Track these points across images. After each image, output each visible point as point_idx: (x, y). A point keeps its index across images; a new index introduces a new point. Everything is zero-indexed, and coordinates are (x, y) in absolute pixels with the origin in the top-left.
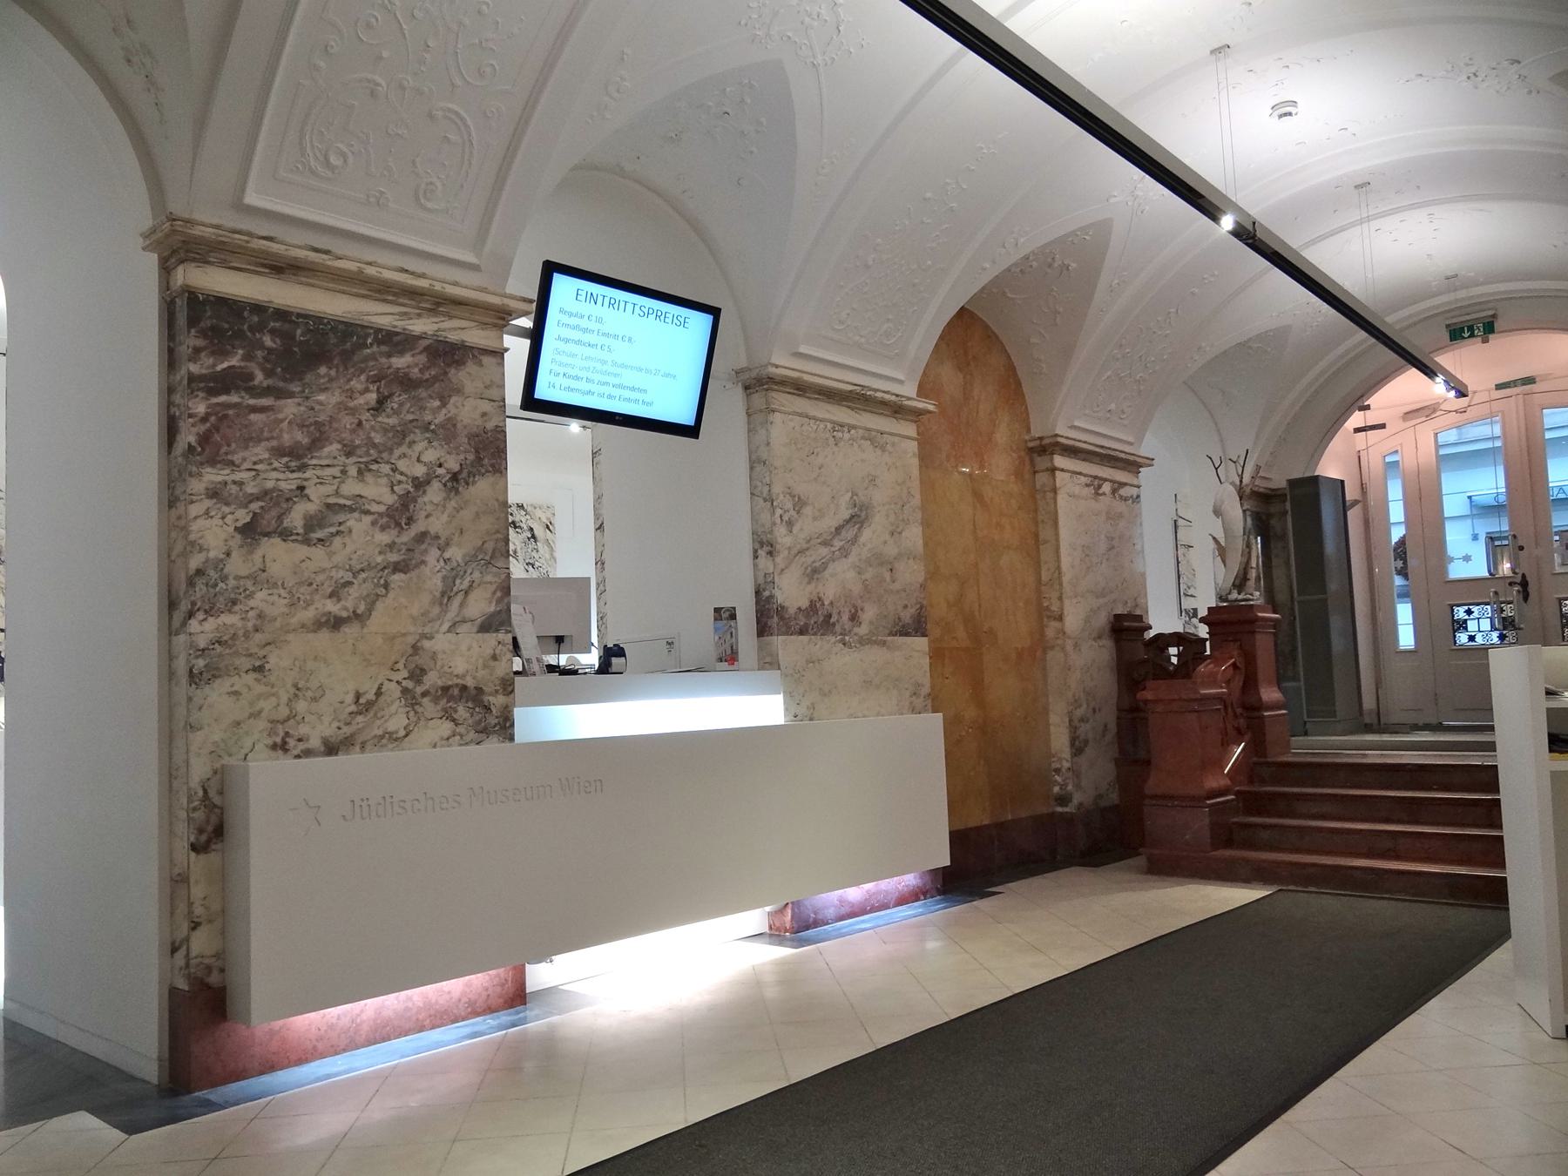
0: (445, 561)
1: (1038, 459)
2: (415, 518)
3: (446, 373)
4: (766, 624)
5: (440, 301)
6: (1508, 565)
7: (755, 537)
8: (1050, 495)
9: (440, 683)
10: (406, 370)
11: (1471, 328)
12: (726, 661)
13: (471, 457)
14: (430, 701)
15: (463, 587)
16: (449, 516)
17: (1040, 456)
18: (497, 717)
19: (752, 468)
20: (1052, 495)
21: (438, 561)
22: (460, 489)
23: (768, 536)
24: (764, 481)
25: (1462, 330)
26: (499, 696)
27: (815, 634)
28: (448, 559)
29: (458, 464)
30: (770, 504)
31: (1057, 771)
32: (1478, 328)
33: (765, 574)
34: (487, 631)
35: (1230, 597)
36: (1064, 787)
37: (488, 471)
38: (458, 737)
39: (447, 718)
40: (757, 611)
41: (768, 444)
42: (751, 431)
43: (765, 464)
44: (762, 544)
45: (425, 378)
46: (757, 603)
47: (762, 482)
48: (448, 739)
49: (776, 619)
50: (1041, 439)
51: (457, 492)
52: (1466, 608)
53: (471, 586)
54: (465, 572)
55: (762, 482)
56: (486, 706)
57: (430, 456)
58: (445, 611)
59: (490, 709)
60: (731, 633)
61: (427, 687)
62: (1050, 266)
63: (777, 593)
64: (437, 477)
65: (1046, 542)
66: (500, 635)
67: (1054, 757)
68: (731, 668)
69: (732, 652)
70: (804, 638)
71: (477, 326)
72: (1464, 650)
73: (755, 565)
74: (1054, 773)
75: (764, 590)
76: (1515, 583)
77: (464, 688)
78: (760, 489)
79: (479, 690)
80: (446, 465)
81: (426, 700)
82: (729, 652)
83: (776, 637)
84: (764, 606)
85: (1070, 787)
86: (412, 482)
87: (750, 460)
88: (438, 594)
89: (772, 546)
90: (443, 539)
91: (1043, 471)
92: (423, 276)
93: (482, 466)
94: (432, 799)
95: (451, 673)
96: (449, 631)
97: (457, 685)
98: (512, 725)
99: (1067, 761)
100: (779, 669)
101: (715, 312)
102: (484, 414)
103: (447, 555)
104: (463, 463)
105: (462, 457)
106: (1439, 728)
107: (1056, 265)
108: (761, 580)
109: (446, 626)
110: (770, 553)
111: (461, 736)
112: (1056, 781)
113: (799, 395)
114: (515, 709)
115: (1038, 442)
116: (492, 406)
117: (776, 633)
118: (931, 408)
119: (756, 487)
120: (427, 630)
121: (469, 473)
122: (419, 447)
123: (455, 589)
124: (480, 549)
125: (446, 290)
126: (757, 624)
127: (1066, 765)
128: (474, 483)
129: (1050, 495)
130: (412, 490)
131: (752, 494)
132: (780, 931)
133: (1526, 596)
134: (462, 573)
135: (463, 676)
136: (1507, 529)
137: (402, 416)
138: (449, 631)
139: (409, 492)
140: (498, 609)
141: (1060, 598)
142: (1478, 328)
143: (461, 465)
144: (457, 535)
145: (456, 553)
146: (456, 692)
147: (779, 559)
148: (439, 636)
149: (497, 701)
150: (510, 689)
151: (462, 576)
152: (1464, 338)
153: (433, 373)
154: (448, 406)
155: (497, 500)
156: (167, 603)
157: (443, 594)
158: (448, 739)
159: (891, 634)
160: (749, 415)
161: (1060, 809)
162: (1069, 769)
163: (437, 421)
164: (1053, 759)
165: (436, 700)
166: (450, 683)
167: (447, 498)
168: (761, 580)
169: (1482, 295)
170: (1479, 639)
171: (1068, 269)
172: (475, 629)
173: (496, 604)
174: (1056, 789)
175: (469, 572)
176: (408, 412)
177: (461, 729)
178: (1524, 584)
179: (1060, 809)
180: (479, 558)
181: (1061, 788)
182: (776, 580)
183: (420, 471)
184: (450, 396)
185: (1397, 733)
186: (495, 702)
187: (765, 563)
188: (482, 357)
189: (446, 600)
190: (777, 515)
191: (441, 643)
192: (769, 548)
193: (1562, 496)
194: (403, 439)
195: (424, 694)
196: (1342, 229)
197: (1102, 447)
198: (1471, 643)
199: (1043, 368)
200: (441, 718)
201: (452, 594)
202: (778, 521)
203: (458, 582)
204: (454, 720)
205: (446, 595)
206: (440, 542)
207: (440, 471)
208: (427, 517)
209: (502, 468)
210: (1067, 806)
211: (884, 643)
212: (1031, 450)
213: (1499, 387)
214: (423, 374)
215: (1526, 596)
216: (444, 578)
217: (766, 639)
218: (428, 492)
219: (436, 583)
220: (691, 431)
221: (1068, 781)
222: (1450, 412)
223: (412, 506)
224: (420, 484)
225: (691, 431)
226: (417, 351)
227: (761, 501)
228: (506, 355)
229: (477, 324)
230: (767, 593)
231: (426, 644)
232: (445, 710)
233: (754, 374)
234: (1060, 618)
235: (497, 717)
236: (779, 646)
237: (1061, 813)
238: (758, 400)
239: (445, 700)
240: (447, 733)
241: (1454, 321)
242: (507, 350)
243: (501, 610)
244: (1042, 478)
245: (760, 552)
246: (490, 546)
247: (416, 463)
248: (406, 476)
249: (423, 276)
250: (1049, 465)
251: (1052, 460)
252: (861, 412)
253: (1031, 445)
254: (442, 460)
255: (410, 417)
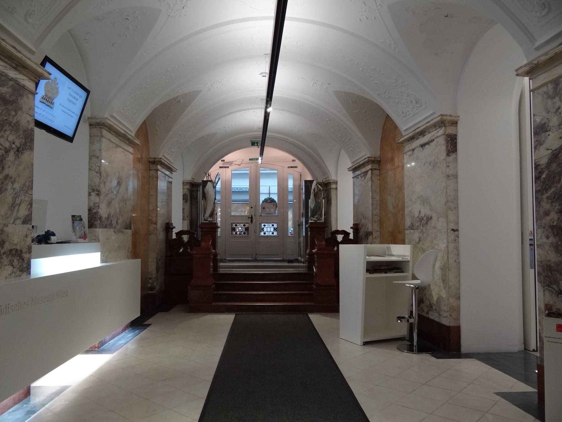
0: (13, 189)
1: (151, 166)
2: (5, 167)
3: (17, 99)
4: (93, 223)
5: (19, 64)
6: (220, 209)
7: (90, 187)
8: (155, 179)
9: (9, 248)
10: (5, 95)
11: (257, 143)
12: (82, 238)
13: (23, 141)
14: (6, 257)
15: (18, 202)
16: (15, 168)
17: (152, 164)
18: (26, 264)
19: (90, 159)
20: (156, 179)
21: (11, 189)
22: (20, 155)
23: (97, 187)
24: (97, 165)
25: (255, 143)
26: (27, 254)
27: (108, 228)
28: (14, 189)
29: (19, 144)
30: (99, 175)
31: (150, 278)
32: (259, 144)
33: (95, 203)
34: (25, 224)
35: (208, 220)
36: (152, 284)
37: (28, 149)
38: (14, 274)
39: (11, 265)
40: (88, 217)
41: (100, 150)
42: (91, 143)
43: (98, 158)
44: (93, 190)
45: (11, 99)
46: (89, 214)
47: (96, 165)
48: (11, 275)
49: (99, 221)
50: (155, 158)
51: (19, 157)
52: (264, 224)
53: (21, 202)
54: (19, 195)
55: (96, 165)
56: (23, 259)
57: (11, 138)
58: (12, 214)
59: (24, 260)
60: (84, 227)
61: (5, 250)
62: (175, 100)
63: (100, 211)
64: (13, 148)
65: (152, 196)
66: (28, 225)
67: (149, 273)
68: (85, 241)
69: (85, 235)
70: (106, 229)
71: (28, 80)
72: (262, 236)
73: (89, 199)
74: (149, 279)
75: (93, 209)
76: (250, 218)
77: (17, 250)
78: (94, 168)
79: (21, 251)
80: (15, 143)
81: (4, 256)
82: (83, 234)
83: (98, 229)
84: (93, 216)
85: (155, 284)
86: (5, 149)
87: (89, 155)
88: (10, 205)
89: (99, 192)
90: (13, 179)
91: (154, 170)
92: (19, 52)
93: (26, 146)
94: (21, 304)
95: (13, 243)
96: (13, 223)
97: (14, 249)
98: (30, 268)
99: (155, 275)
100: (99, 242)
101: (88, 92)
102: (28, 122)
103: (14, 187)
104: (21, 143)
105: (21, 140)
106: (255, 260)
107: (177, 100)
108: (92, 205)
109: (12, 222)
110: (98, 195)
111: (15, 273)
112: (149, 282)
113: (109, 132)
114: (32, 260)
115: (153, 160)
116: (31, 118)
117: (99, 227)
118: (139, 144)
119: (92, 167)
120: (6, 222)
121: (23, 148)
122: (8, 133)
123: (16, 203)
124: (24, 185)
125: (26, 61)
126: (88, 223)
127: (154, 276)
128: (24, 153)
129: (155, 179)
130: (4, 153)
131: (90, 169)
132: (92, 348)
133: (252, 221)
134: (18, 195)
135: (16, 245)
136: (220, 198)
137: (2, 117)
138: (13, 223)
139: (3, 154)
140: (28, 213)
141: (156, 216)
142: (259, 144)
143: (20, 144)
144: (18, 177)
145: (17, 186)
146: (14, 252)
147: (101, 197)
148: (10, 225)
149: (26, 256)
150: (30, 251)
151: (18, 197)
152: (255, 145)
153: (13, 98)
154: (17, 115)
155: (30, 163)
156: (459, 224)
157: (12, 205)
158: (11, 275)
159: (125, 229)
160: (90, 136)
161: (150, 292)
162: (155, 278)
163: (14, 122)
164: (149, 274)
165: (7, 257)
166: (12, 248)
167: (15, 159)
168: (92, 205)
169: (271, 135)
170: (267, 234)
171: (180, 102)
172: (21, 223)
173: (28, 211)
174: (149, 285)
175: (20, 195)
176: (5, 115)
177: (15, 270)
178: (252, 218)
179: (150, 292)
180: (24, 189)
181: (151, 285)
182: (100, 205)
183: (7, 145)
184: (18, 111)
185: (224, 262)
186: (26, 257)
187: (94, 198)
188: (28, 94)
189: (13, 208)
190: (102, 180)
191: (10, 229)
192: (98, 192)
193: (237, 190)
194: (3, 128)
195: (4, 253)
196: (248, 109)
197: (169, 164)
198: (272, 235)
199: (158, 133)
200: (9, 265)
201: (15, 205)
202: (102, 181)
203: (17, 199)
204: (13, 266)
205: (13, 206)
206: (12, 180)
207: (14, 146)
208: (9, 167)
209: (33, 148)
210: (153, 291)
211: (122, 232)
212: (149, 162)
213: (250, 160)
214: (10, 98)
215: (252, 221)
216: (13, 197)
217: (92, 229)
218: (9, 155)
219: (10, 200)
220: (70, 139)
221: (154, 282)
222: (236, 164)
223: (4, 161)
224: (7, 151)
225: (70, 139)
226: (8, 86)
227: (94, 173)
228: (36, 95)
229: (28, 79)
230: (95, 211)
231: (5, 228)
232: (10, 261)
233: (98, 121)
234: (156, 224)
235: (26, 264)
236: (100, 233)
237: (151, 294)
238: (96, 131)
239: (10, 256)
240: (10, 272)
241: (254, 140)
242: (37, 94)
243: (29, 214)
244: (153, 173)
245: (92, 193)
246: (27, 184)
247: (6, 140)
248: (3, 146)
249: (19, 52)
250: (156, 168)
251: (157, 167)
252: (122, 142)
253: (150, 160)
254: (14, 141)
255: (5, 118)
